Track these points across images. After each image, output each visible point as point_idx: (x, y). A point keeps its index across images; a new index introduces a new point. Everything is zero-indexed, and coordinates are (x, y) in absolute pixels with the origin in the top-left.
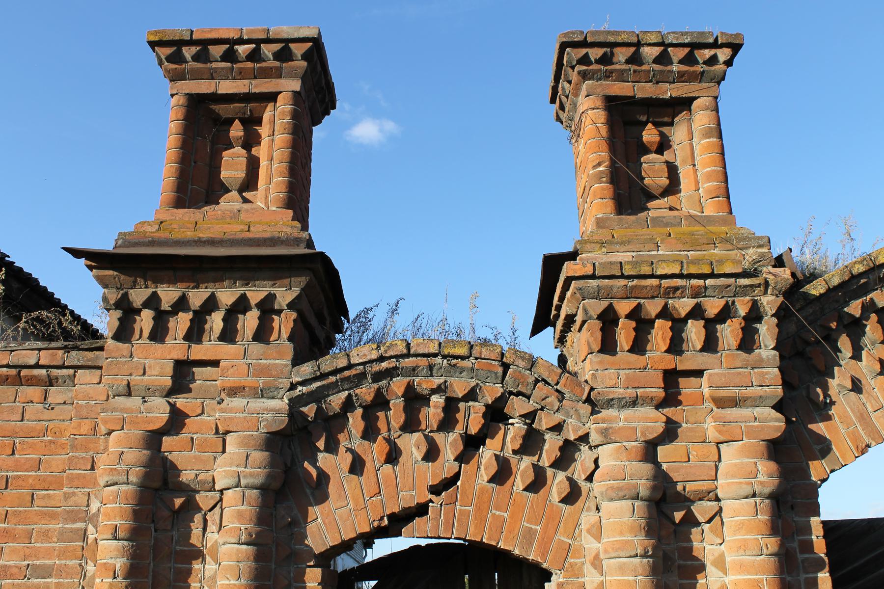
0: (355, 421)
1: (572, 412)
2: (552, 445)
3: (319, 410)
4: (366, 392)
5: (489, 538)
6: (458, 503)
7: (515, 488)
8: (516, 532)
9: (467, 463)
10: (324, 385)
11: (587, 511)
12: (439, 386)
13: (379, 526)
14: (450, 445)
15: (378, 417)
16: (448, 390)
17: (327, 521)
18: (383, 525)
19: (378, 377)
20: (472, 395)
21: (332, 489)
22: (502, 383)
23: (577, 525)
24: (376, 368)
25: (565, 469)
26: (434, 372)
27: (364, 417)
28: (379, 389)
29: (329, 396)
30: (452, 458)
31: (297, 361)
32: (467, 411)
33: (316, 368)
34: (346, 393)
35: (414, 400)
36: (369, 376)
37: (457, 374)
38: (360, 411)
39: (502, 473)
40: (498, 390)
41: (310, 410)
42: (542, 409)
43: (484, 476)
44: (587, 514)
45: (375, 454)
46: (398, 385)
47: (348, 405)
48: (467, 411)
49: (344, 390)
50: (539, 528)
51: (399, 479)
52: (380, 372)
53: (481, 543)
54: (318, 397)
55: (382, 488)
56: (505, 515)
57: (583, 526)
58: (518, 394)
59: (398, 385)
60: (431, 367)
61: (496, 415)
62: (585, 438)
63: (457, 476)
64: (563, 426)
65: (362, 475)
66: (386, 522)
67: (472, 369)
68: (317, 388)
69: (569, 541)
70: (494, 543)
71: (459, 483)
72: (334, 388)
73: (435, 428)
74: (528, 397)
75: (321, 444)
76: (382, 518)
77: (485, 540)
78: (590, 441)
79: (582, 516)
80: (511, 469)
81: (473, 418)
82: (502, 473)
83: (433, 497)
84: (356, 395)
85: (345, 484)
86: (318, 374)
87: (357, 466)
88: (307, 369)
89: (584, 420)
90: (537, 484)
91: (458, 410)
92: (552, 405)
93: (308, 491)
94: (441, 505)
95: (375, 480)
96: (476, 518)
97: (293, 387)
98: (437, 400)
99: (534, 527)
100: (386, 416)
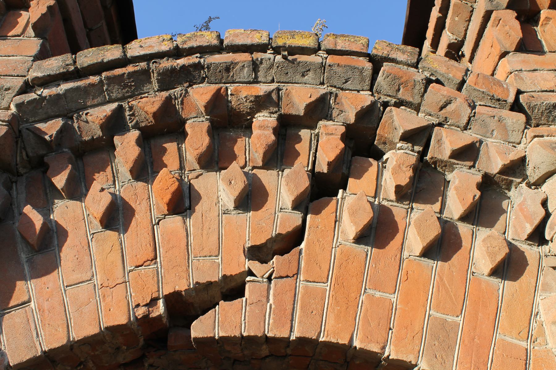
0: (127, 147)
1: (493, 124)
2: (461, 188)
3: (64, 131)
4: (149, 104)
5: (366, 338)
6: (302, 277)
7: (406, 254)
8: (417, 328)
9: (317, 212)
10: (78, 88)
11: (544, 290)
12: (268, 95)
13: (146, 317)
14: (285, 187)
15: (165, 150)
16: (283, 104)
17: (46, 305)
18: (154, 315)
19: (169, 79)
20: (320, 110)
21: (67, 253)
22: (371, 90)
23: (532, 315)
24: (166, 64)
25: (490, 224)
26: (261, 74)
27: (140, 142)
28: (169, 99)
29: (86, 108)
30: (289, 205)
31: (42, 55)
32: (314, 142)
33: (70, 61)
34: (115, 105)
35: (227, 122)
36: (154, 78)
37: (298, 78)
38: (135, 134)
39: (378, 231)
40: (366, 99)
41: (51, 128)
42: (440, 125)
43: (350, 228)
44: (545, 295)
45: (153, 200)
46: (200, 94)
47: (115, 124)
48: (314, 142)
49: (111, 101)
50: (460, 320)
51: (191, 238)
52: (173, 70)
53: (350, 346)
54: (67, 107)
55: (161, 252)
56: (394, 298)
57: (542, 317)
58: (399, 104)
59: (200, 94)
60: (255, 66)
61: (362, 144)
62: (517, 168)
63: (296, 237)
64: (478, 150)
65: (126, 230)
66: (160, 308)
67: (322, 66)
68: (67, 91)
69: (524, 344)
70: (375, 348)
71: (303, 245)
72: (96, 94)
73: (260, 164)
74: (417, 109)
75: (60, 181)
76: (153, 302)
77: (357, 344)
78: (528, 173)
79: (538, 299)
80: (396, 222)
81: (325, 144)
82: (378, 231)
83: (255, 266)
84: (131, 108)
85: (93, 245)
86: (72, 68)
87: (117, 216)
88: (55, 64)
89: (515, 138)
90: (443, 246)
91: (299, 139)
92: (456, 113)
93: (23, 257)
94: (269, 279)
95: (149, 238)
96: (337, 303)
97: (27, 88)
98: (264, 122)
99: (450, 318)
100: (179, 149)
